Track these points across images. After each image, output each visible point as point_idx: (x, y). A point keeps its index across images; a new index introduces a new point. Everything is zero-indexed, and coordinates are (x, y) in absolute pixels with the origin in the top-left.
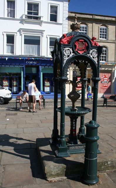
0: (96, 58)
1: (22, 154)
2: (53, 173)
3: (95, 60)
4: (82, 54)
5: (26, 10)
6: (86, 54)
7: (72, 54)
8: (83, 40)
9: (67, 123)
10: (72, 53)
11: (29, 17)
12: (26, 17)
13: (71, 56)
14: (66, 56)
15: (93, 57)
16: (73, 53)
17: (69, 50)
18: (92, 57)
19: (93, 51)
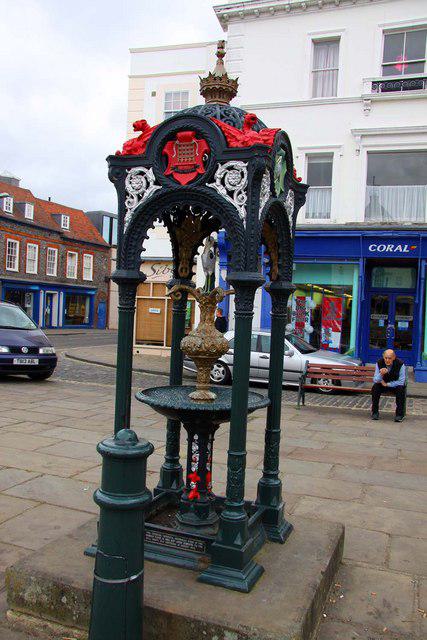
0: (240, 193)
1: (115, 579)
2: (26, 596)
3: (235, 203)
4: (189, 183)
5: (379, 60)
6: (202, 184)
7: (154, 188)
8: (190, 133)
9: (421, 414)
10: (151, 184)
11: (387, 87)
12: (374, 88)
13: (148, 193)
14: (132, 197)
15: (231, 193)
16: (156, 183)
17: (142, 173)
18: (222, 191)
19: (231, 168)
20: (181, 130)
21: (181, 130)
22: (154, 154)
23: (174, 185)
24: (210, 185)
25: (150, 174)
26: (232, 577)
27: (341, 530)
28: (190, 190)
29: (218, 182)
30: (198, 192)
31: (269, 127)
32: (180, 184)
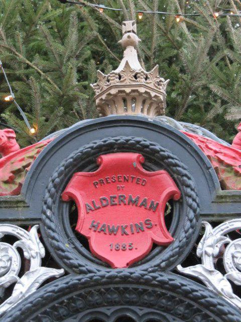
4: (133, 264)
7: (39, 273)
8: (134, 156)
10: (35, 263)
16: (47, 261)
17: (10, 239)
18: (219, 283)
20: (109, 148)
21: (109, 148)
22: (45, 190)
23: (92, 267)
24: (188, 270)
25: (31, 242)
26: (66, 210)
27: (142, 229)
28: (138, 280)
29: (208, 263)
30: (162, 284)
31: (124, 51)
32: (109, 265)
